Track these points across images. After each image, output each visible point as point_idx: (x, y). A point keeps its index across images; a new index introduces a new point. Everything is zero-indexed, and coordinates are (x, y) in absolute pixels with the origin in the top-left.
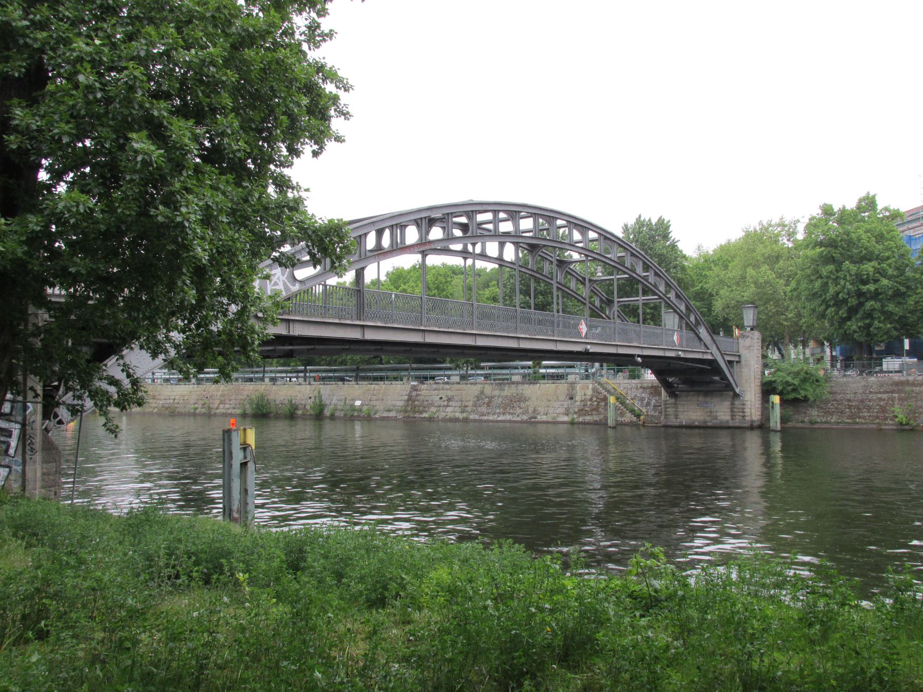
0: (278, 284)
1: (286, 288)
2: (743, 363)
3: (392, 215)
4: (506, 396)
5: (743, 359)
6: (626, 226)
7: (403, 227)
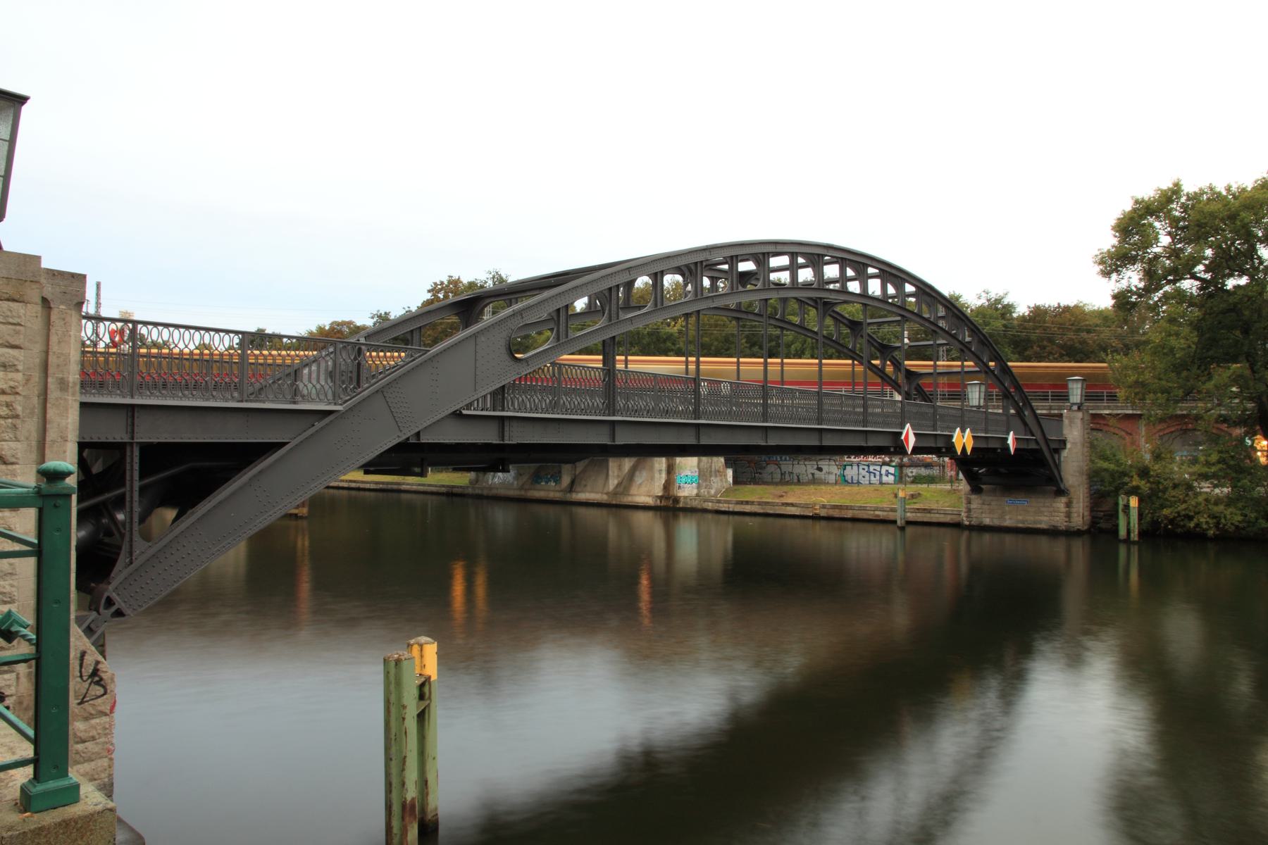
3: (660, 257)
6: (960, 297)
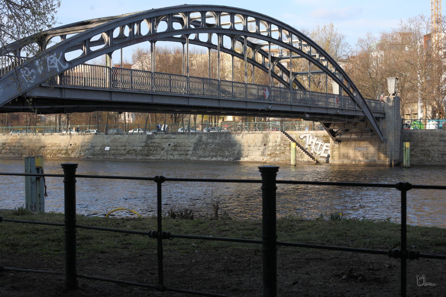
0: (54, 65)
1: (60, 67)
2: (387, 119)
4: (218, 143)
5: (387, 116)
7: (139, 23)
